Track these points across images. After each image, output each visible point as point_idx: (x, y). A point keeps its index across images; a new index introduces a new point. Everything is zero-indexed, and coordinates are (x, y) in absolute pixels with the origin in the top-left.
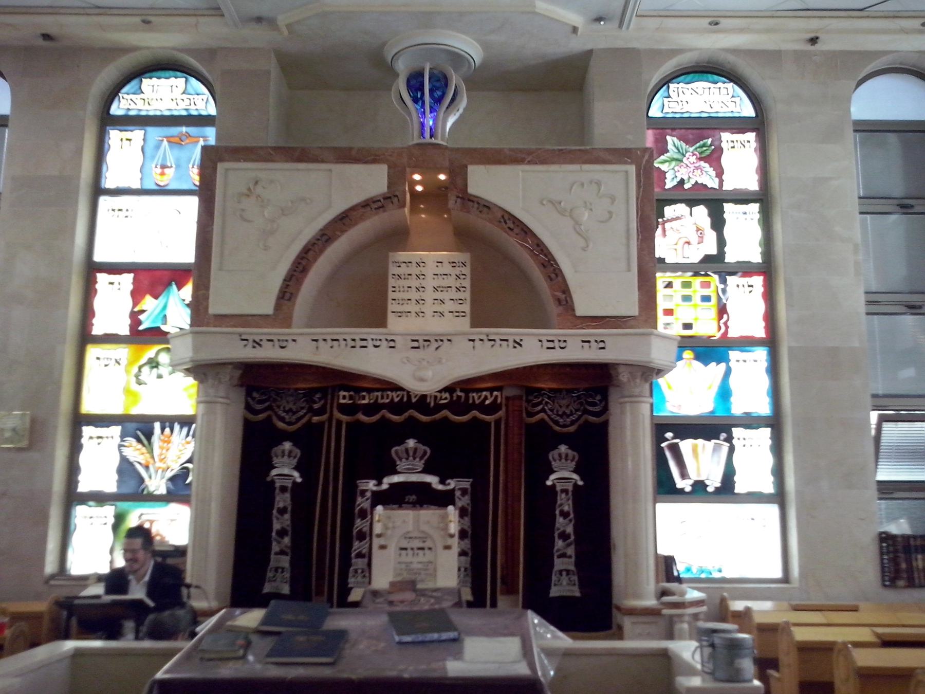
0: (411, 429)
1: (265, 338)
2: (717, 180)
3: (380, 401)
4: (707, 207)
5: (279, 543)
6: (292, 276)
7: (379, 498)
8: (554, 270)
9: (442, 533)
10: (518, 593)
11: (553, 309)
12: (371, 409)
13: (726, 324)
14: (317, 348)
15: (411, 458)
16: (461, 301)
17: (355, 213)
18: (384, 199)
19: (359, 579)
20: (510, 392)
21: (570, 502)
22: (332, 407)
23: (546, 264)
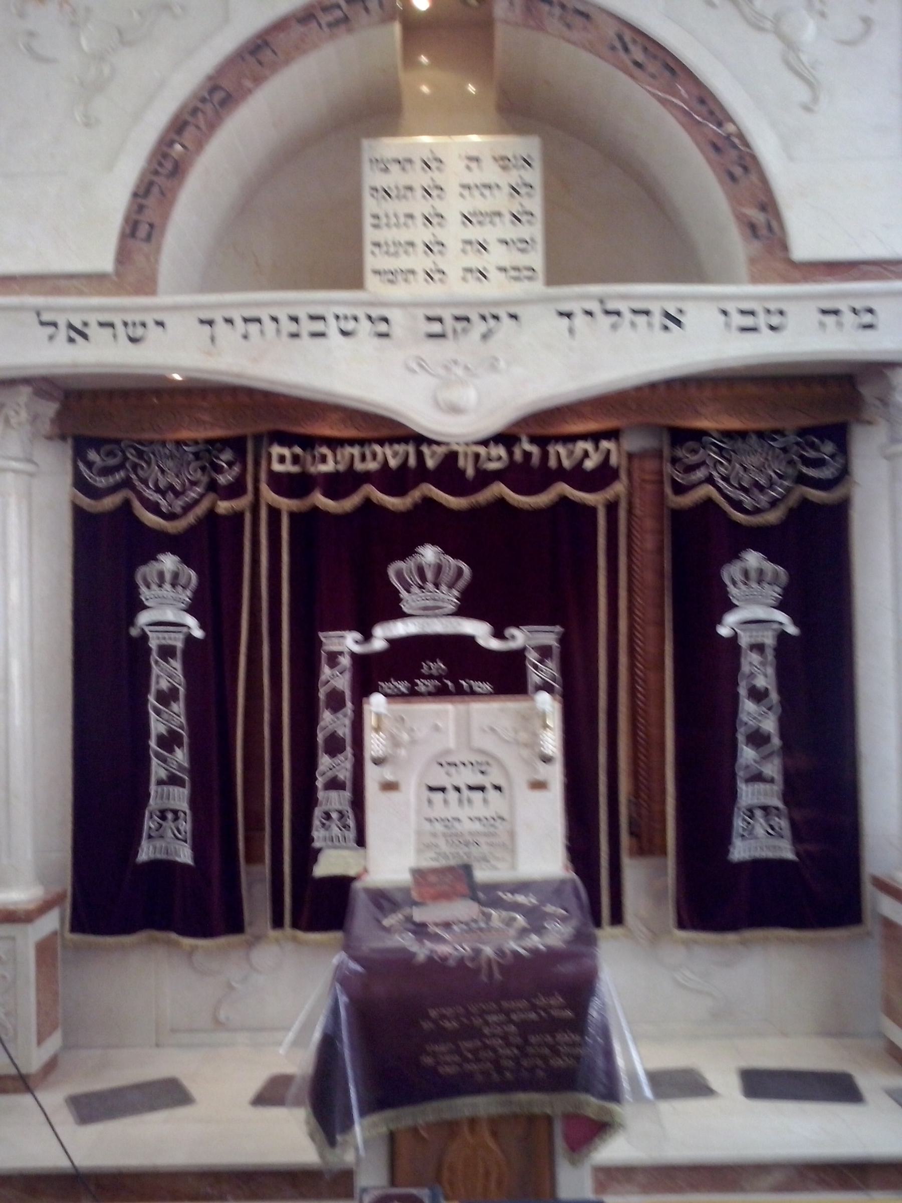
0: (428, 524)
1: (93, 319)
3: (359, 466)
5: (164, 760)
6: (151, 184)
7: (369, 674)
8: (741, 157)
9: (525, 753)
10: (664, 852)
11: (738, 247)
14: (213, 339)
15: (430, 586)
16: (524, 244)
17: (282, 36)
19: (335, 830)
20: (633, 443)
21: (770, 671)
22: (256, 481)
23: (720, 143)
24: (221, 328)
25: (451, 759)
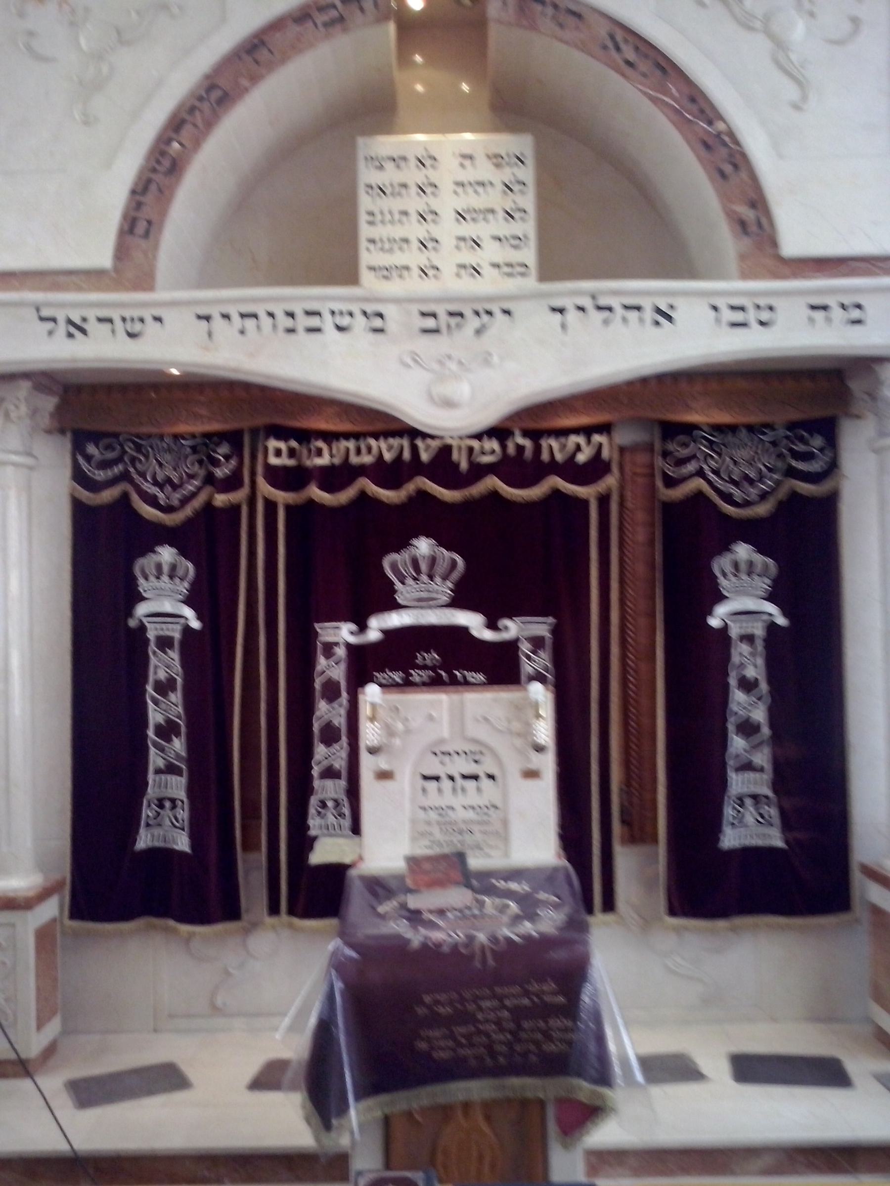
0: (422, 516)
1: (91, 314)
3: (354, 460)
5: (162, 749)
6: (149, 181)
7: (364, 664)
8: (731, 155)
9: (518, 742)
10: (655, 840)
11: (728, 243)
14: (210, 334)
15: (424, 578)
16: (517, 241)
17: (278, 35)
19: (331, 819)
20: (624, 436)
21: (760, 661)
22: (253, 474)
23: (710, 141)
24: (218, 323)
25: (445, 748)
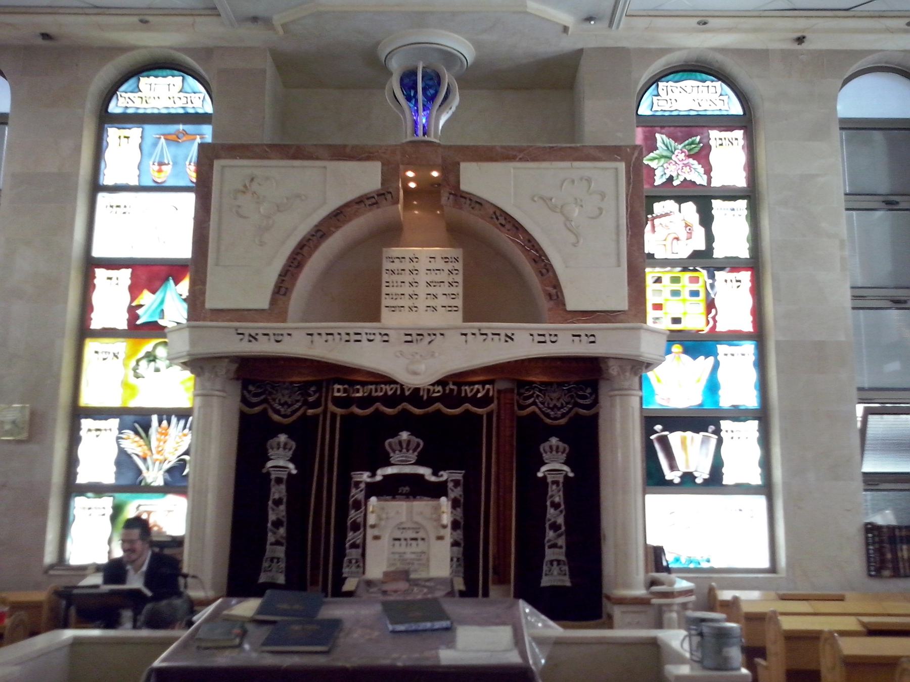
0: (405, 421)
1: (260, 332)
2: (705, 177)
3: (374, 394)
4: (695, 203)
5: (274, 533)
6: (287, 271)
7: (373, 490)
8: (545, 265)
9: (435, 523)
10: (509, 582)
11: (544, 304)
12: (365, 402)
13: (714, 318)
14: (312, 342)
15: (404, 450)
16: (454, 296)
17: (349, 209)
18: (378, 195)
19: (354, 569)
20: (501, 385)
21: (561, 493)
22: (326, 400)
23: (537, 259)
